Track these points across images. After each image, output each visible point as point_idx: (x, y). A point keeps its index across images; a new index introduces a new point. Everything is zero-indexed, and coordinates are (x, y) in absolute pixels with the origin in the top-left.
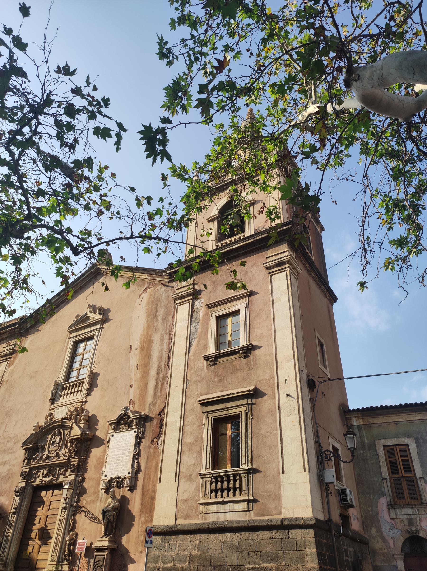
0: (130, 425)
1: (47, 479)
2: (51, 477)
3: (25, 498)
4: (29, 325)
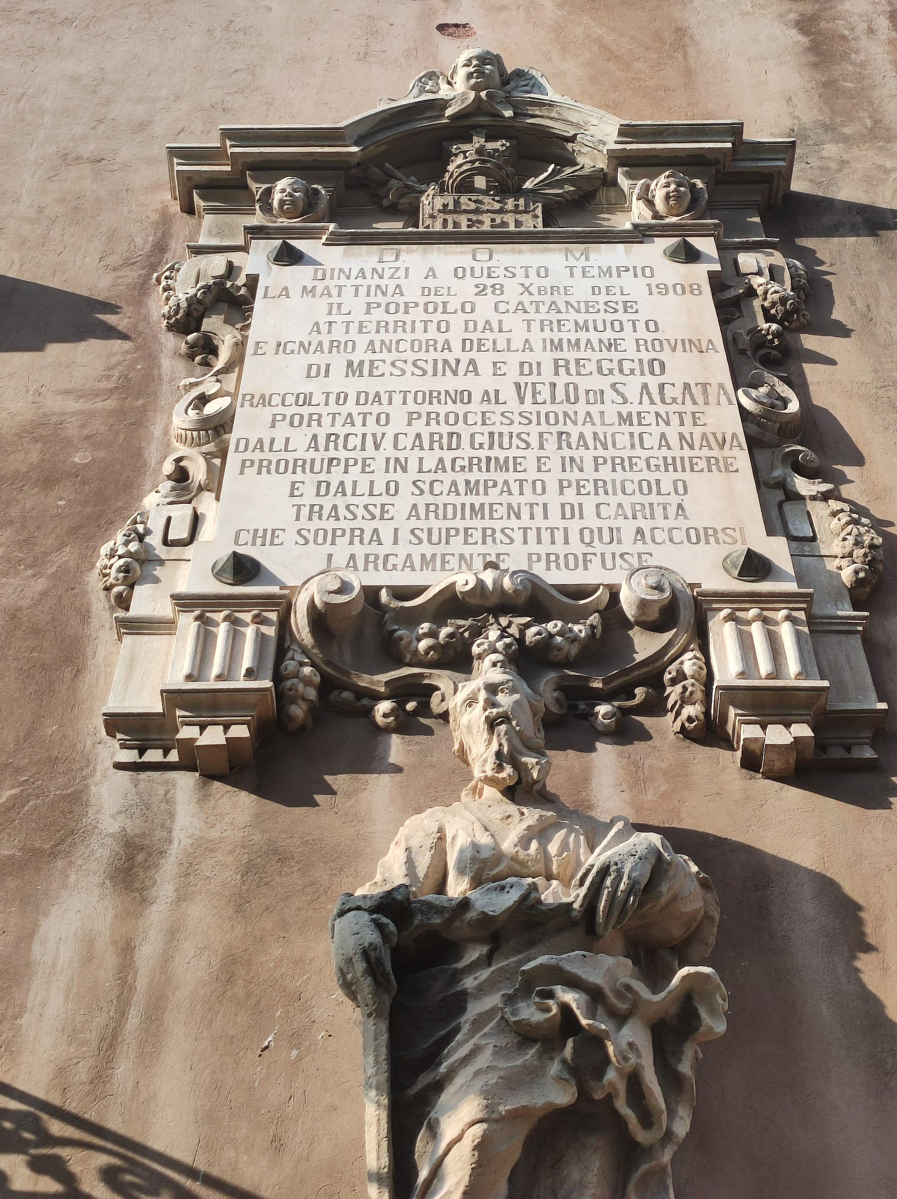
0: (577, 210)
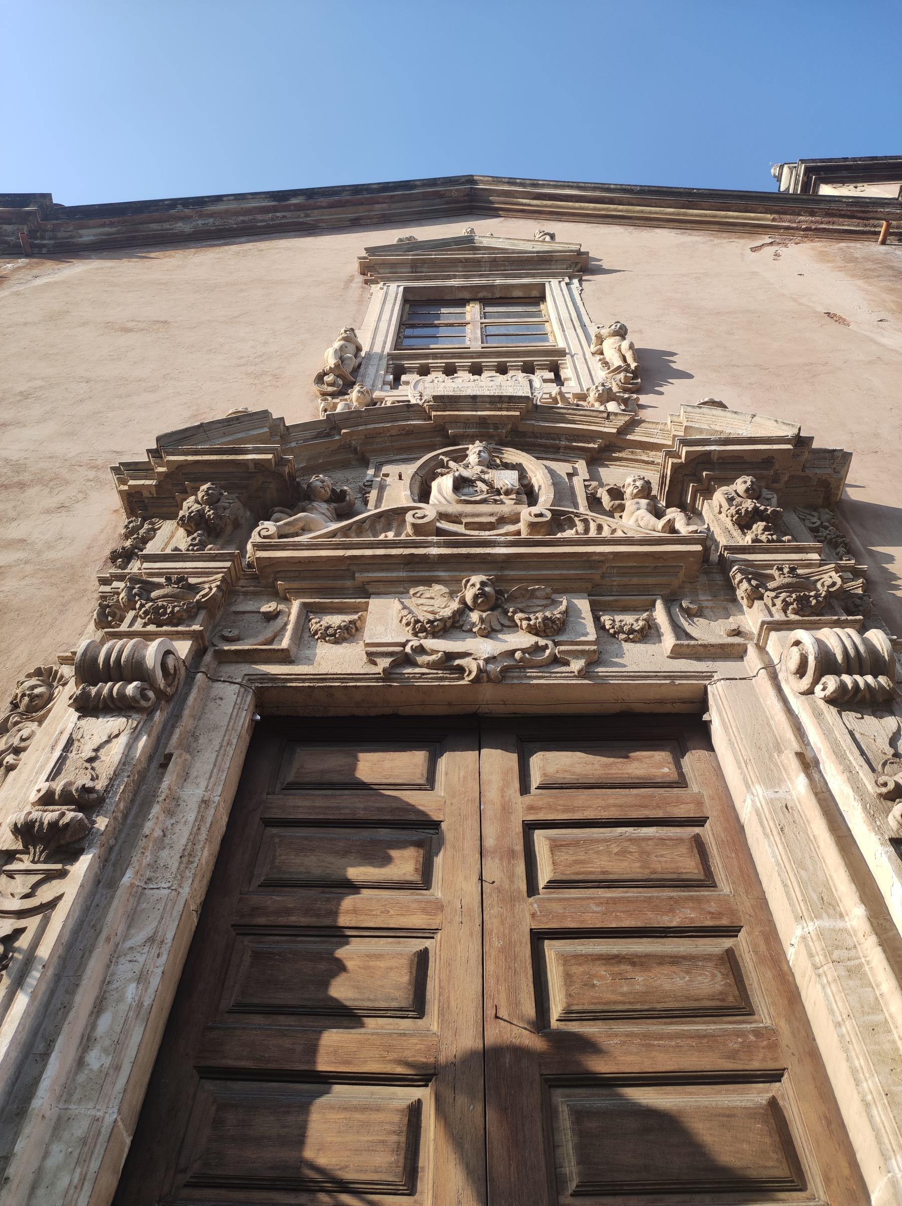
1: (479, 649)
3: (190, 745)
4: (88, 235)
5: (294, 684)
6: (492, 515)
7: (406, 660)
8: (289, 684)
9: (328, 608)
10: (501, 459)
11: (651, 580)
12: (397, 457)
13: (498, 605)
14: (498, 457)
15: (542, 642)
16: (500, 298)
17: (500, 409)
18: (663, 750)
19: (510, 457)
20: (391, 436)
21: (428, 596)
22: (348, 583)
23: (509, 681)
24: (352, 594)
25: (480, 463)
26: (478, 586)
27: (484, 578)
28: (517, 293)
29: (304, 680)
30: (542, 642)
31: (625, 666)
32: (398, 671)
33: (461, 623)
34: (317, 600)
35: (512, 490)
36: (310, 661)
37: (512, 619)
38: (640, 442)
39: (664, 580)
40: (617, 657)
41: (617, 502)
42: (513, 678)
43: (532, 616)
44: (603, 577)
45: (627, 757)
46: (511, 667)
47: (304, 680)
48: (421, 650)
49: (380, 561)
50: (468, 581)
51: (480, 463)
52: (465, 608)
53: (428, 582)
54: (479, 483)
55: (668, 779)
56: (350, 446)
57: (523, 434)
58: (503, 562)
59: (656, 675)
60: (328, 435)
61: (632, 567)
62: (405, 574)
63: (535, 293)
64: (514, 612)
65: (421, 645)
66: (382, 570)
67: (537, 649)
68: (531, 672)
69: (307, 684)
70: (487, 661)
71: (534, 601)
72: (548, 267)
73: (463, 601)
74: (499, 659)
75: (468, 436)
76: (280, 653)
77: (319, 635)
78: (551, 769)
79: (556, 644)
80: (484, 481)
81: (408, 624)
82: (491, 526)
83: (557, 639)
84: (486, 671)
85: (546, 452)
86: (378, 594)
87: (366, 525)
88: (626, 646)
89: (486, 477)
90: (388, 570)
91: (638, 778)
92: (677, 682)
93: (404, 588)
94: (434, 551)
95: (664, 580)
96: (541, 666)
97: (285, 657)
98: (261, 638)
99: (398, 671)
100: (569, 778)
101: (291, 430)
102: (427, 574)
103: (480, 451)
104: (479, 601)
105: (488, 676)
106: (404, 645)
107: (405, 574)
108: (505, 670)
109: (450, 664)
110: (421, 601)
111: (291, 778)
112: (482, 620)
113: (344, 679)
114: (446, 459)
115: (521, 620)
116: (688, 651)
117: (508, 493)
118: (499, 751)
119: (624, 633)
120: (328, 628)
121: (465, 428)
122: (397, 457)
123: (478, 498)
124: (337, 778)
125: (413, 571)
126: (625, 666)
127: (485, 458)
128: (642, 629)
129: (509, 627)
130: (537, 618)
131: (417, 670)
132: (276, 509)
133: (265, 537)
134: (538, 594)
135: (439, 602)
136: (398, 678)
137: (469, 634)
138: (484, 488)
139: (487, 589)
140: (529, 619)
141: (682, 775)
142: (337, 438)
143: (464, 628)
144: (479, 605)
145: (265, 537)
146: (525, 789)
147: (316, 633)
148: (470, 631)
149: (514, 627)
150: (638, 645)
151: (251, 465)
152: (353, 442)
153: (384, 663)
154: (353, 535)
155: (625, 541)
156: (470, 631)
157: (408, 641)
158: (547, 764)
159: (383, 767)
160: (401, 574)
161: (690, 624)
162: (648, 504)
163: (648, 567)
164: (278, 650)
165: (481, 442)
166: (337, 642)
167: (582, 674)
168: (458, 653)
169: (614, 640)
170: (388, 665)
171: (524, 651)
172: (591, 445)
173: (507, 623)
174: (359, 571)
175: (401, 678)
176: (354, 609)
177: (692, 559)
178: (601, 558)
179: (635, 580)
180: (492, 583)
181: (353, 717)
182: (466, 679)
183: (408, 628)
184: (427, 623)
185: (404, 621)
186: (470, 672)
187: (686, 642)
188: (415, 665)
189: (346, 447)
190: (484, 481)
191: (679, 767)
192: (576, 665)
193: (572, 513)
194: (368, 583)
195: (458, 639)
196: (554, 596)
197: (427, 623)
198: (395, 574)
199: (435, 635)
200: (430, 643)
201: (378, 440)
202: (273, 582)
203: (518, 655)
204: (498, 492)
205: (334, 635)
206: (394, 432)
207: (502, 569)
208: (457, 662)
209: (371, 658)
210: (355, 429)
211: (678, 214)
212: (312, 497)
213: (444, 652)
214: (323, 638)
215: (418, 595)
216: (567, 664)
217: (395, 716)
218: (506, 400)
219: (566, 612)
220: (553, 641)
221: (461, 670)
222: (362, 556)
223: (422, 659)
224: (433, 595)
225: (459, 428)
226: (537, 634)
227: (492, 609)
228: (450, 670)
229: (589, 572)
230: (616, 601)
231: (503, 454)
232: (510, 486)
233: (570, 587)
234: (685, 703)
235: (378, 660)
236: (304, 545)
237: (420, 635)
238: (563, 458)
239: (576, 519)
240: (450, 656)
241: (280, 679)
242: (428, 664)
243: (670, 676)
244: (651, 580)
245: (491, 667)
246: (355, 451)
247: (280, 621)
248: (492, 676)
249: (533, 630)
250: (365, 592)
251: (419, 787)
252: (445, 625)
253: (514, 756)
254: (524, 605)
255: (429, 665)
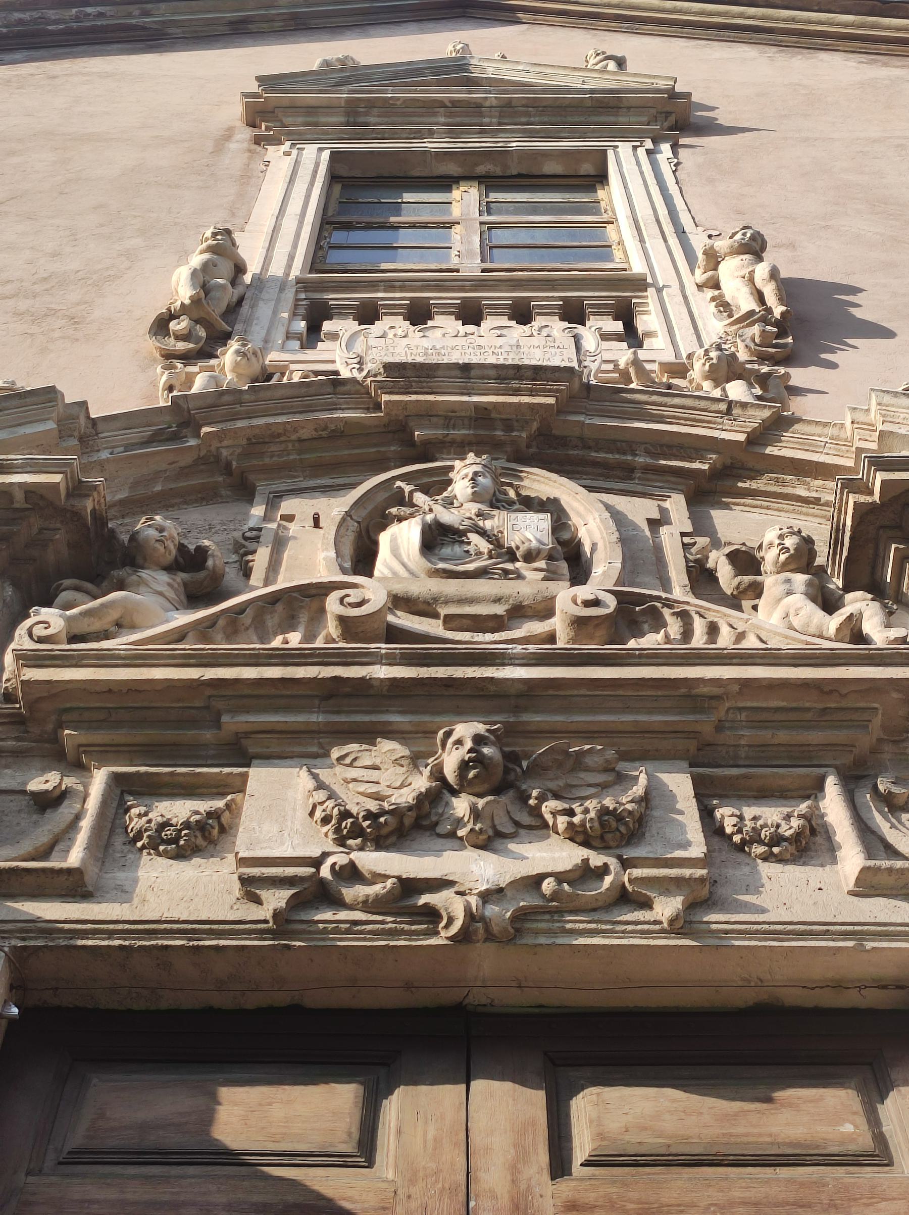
2: (551, 855)
5: (90, 943)
6: (498, 600)
7: (316, 892)
8: (80, 942)
9: (166, 785)
10: (517, 490)
11: (815, 737)
12: (312, 483)
13: (509, 783)
14: (510, 485)
15: (597, 859)
16: (520, 176)
17: (516, 392)
18: (842, 1086)
19: (536, 486)
20: (300, 440)
21: (368, 763)
22: (208, 735)
23: (529, 940)
24: (213, 757)
25: (476, 497)
26: (469, 744)
27: (480, 728)
28: (551, 168)
29: (110, 934)
30: (597, 859)
31: (764, 911)
32: (304, 916)
33: (434, 818)
34: (143, 769)
35: (539, 551)
36: (124, 894)
37: (536, 812)
38: (792, 460)
39: (840, 736)
40: (747, 892)
41: (748, 579)
42: (537, 933)
43: (578, 810)
44: (720, 727)
45: (769, 1100)
46: (536, 908)
47: (110, 934)
48: (351, 874)
49: (273, 691)
50: (448, 734)
51: (476, 497)
52: (441, 790)
53: (368, 735)
54: (474, 538)
55: (852, 1148)
56: (217, 458)
57: (563, 442)
58: (519, 696)
59: (826, 930)
60: (175, 437)
61: (777, 710)
62: (321, 718)
63: (587, 168)
64: (542, 799)
65: (352, 864)
66: (276, 710)
67: (587, 874)
68: (573, 922)
69: (117, 943)
70: (486, 896)
71: (582, 775)
72: (612, 119)
73: (438, 774)
74: (509, 893)
75: (453, 443)
76: (63, 878)
77: (145, 840)
78: (614, 1124)
79: (626, 864)
80: (483, 533)
81: (326, 820)
82: (495, 624)
83: (629, 853)
84: (482, 919)
85: (607, 477)
86: (269, 758)
87: (247, 618)
88: (766, 869)
89: (488, 524)
90: (287, 709)
91: (791, 1144)
92: (869, 945)
93: (321, 746)
94: (382, 672)
95: (840, 736)
96: (594, 910)
97: (73, 886)
98: (27, 846)
99: (304, 916)
100: (651, 1142)
101: (100, 426)
102: (366, 718)
103: (476, 474)
104: (471, 775)
105: (487, 929)
106: (317, 863)
107: (321, 718)
108: (521, 917)
109: (410, 902)
110: (353, 773)
111: (77, 1139)
112: (476, 814)
113: (194, 931)
114: (407, 488)
115: (554, 814)
116: (890, 880)
117: (530, 557)
118: (508, 1085)
119: (761, 842)
120: (165, 825)
121: (447, 427)
122: (312, 483)
123: (471, 567)
124: (172, 1140)
125: (338, 712)
126: (764, 911)
127: (485, 488)
128: (798, 835)
129: (530, 828)
130: (586, 811)
131: (343, 915)
132: (67, 582)
133: (41, 640)
134: (589, 761)
135: (389, 776)
136: (303, 932)
137: (449, 843)
138: (484, 546)
139: (486, 750)
140: (571, 813)
141: (880, 1139)
142: (192, 442)
143: (440, 830)
144: (471, 782)
145: (41, 640)
146: (560, 1166)
147: (139, 836)
148: (452, 835)
149: (540, 827)
150: (790, 868)
151: (19, 496)
152: (225, 453)
153: (276, 899)
154: (219, 637)
155: (763, 657)
156: (452, 835)
157: (325, 855)
158: (607, 1112)
159: (255, 1115)
160: (314, 718)
161: (893, 826)
162: (809, 584)
163: (808, 709)
164: (61, 871)
165: (478, 455)
166: (180, 855)
167: (681, 925)
168: (427, 880)
169: (741, 857)
170: (283, 904)
171: (560, 877)
172: (697, 465)
173: (526, 819)
174: (229, 711)
175: (310, 930)
176: (218, 788)
177: (895, 695)
178: (716, 691)
179: (783, 737)
180: (498, 738)
181: (209, 1012)
182: (443, 934)
183: (325, 829)
184: (365, 818)
185: (319, 814)
186: (451, 921)
187: (885, 864)
188: (339, 903)
189: (210, 461)
190: (483, 533)
191: (874, 1121)
192: (666, 908)
193: (658, 599)
194: (248, 734)
195: (426, 852)
196: (622, 766)
197: (365, 818)
198: (301, 718)
199: (380, 842)
200: (370, 860)
201: (273, 448)
202: (55, 732)
203: (548, 886)
204: (511, 555)
205: (175, 840)
206: (305, 433)
207: (517, 709)
208: (424, 899)
209: (251, 888)
210: (228, 426)
211: (863, 26)
212: (139, 560)
213: (399, 878)
214: (153, 846)
215: (348, 761)
216: (647, 904)
217: (296, 1010)
218: (529, 374)
219: (645, 800)
220: (620, 858)
221: (432, 915)
222: (237, 681)
223: (353, 892)
224: (378, 761)
225: (436, 427)
226: (586, 844)
227: (497, 791)
228: (410, 914)
229: (691, 718)
230: (746, 777)
231: (521, 479)
232: (534, 544)
233: (652, 748)
234: (884, 987)
235: (264, 894)
236: (119, 657)
237: (350, 842)
238: (639, 488)
239: (666, 612)
240: (410, 887)
241: (61, 931)
242: (365, 902)
243: (854, 933)
244: (815, 737)
245: (492, 910)
246: (227, 469)
247: (66, 811)
248: (495, 929)
249: (579, 836)
250: (241, 753)
251: (341, 1161)
252: (401, 823)
253: (539, 1097)
254: (561, 783)
255: (367, 905)
